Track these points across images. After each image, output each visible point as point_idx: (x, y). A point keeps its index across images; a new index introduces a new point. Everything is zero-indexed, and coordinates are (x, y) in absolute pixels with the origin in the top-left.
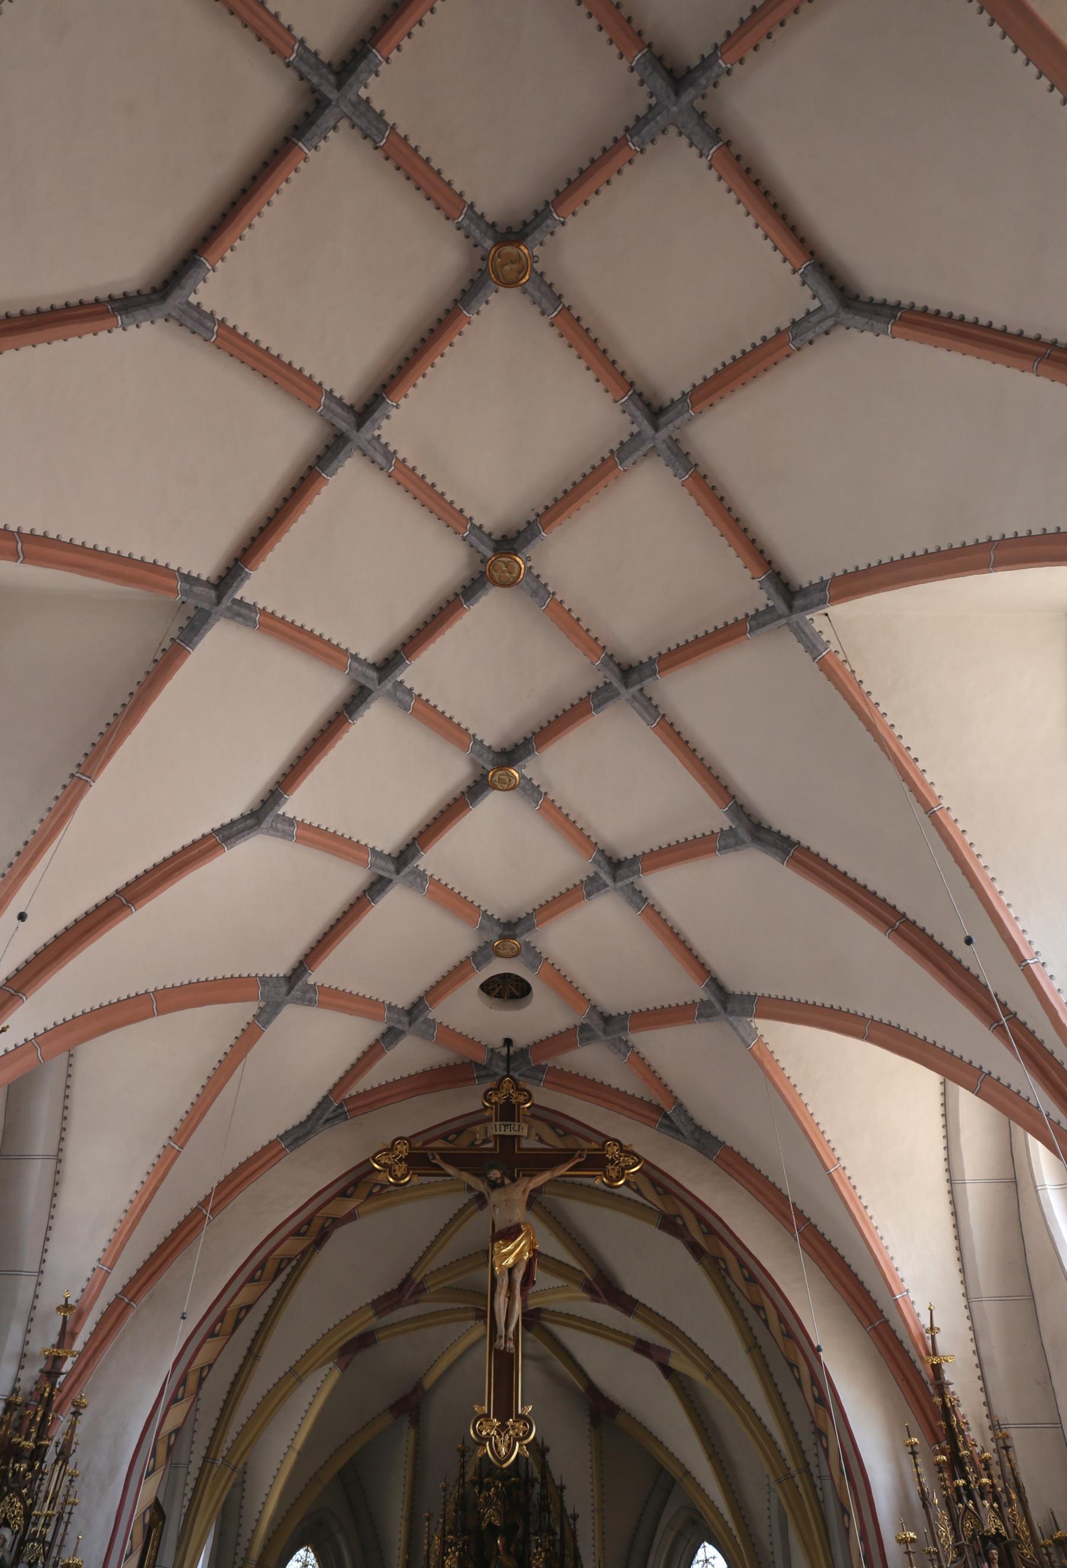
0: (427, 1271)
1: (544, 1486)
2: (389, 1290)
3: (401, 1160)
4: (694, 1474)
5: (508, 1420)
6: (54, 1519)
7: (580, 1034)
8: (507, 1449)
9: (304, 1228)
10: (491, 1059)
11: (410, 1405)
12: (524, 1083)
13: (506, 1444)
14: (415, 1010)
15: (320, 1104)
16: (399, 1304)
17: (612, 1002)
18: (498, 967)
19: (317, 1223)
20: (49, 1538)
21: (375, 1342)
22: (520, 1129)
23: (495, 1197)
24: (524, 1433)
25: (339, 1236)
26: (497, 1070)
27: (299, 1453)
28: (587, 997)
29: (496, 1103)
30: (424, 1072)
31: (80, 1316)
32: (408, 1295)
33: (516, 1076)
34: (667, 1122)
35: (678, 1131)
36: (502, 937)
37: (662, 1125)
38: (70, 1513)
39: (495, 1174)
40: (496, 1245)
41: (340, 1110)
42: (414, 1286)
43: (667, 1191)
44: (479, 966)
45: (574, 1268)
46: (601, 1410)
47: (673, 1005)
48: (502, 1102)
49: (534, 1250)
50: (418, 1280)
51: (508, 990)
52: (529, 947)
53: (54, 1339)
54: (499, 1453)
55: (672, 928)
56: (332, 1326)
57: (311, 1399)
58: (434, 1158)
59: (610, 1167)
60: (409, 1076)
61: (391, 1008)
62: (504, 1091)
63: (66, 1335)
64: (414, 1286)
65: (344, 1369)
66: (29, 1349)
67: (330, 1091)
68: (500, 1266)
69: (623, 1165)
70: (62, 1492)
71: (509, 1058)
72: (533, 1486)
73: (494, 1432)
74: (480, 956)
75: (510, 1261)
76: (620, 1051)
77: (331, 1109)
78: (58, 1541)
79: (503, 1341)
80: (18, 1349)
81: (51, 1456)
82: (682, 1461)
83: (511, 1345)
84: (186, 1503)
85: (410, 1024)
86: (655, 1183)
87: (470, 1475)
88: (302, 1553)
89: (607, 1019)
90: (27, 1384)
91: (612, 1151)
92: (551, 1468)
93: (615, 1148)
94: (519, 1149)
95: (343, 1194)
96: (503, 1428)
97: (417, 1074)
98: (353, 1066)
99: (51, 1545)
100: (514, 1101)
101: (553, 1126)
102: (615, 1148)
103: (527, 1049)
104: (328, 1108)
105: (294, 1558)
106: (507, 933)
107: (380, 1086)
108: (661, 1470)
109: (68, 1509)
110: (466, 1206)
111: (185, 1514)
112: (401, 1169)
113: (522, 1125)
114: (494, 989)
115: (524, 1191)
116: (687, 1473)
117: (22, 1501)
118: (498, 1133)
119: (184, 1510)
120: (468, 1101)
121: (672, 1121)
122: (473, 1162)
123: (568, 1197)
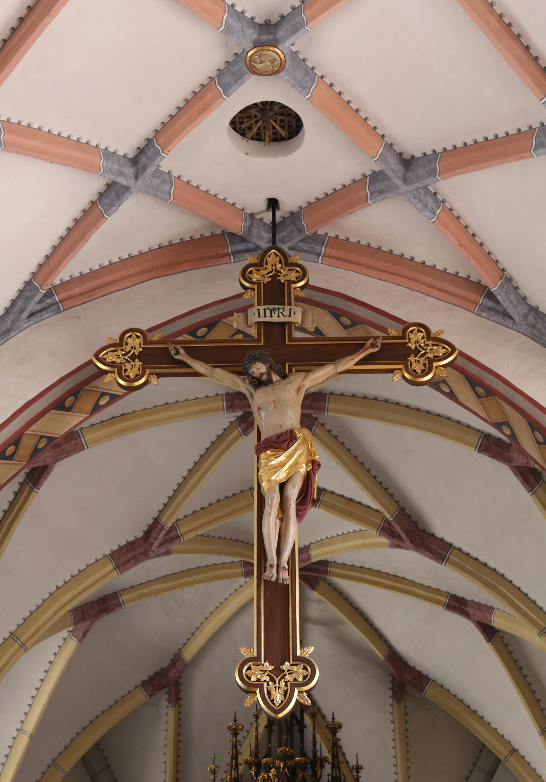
0: (179, 514)
1: (335, 765)
2: (131, 539)
3: (133, 357)
4: (522, 752)
5: (283, 664)
7: (373, 185)
8: (282, 699)
9: (11, 449)
10: (250, 227)
11: (168, 680)
12: (295, 257)
13: (282, 691)
14: (141, 158)
15: (21, 292)
16: (146, 555)
17: (415, 140)
18: (254, 91)
19: (27, 445)
21: (119, 605)
22: (295, 315)
23: (259, 398)
24: (305, 677)
25: (64, 473)
26: (259, 243)
27: (31, 736)
28: (380, 132)
29: (258, 283)
30: (161, 247)
32: (157, 543)
33: (285, 248)
34: (491, 304)
35: (506, 315)
36: (258, 44)
37: (483, 308)
39: (259, 369)
40: (262, 456)
41: (49, 301)
42: (163, 533)
43: (490, 392)
44: (227, 89)
45: (369, 507)
46: (405, 681)
47: (501, 134)
48: (267, 280)
49: (313, 462)
50: (169, 525)
51: (270, 126)
52: (299, 61)
54: (272, 701)
55: (501, 16)
56: (61, 584)
57: (42, 675)
58: (178, 353)
59: (412, 359)
60: (141, 254)
61: (108, 154)
62: (269, 267)
64: (163, 533)
67: (34, 274)
68: (269, 480)
69: (430, 355)
71: (274, 227)
72: (322, 766)
73: (266, 678)
74: (227, 76)
75: (281, 475)
76: (426, 206)
77: (37, 298)
79: (274, 570)
82: (507, 737)
83: (285, 575)
85: (136, 177)
86: (473, 382)
87: (245, 755)
89: (408, 163)
91: (416, 339)
92: (345, 749)
93: (421, 335)
94: (291, 339)
95: (59, 405)
96: (278, 672)
97: (151, 250)
98: (62, 239)
100: (282, 279)
101: (336, 314)
102: (421, 335)
103: (299, 213)
104: (33, 297)
106: (264, 38)
107: (102, 268)
108: (482, 748)
110: (226, 431)
112: (133, 368)
113: (294, 308)
114: (250, 128)
115: (298, 390)
116: (514, 751)
118: (262, 319)
120: (221, 283)
121: (498, 302)
122: (231, 357)
123: (357, 414)
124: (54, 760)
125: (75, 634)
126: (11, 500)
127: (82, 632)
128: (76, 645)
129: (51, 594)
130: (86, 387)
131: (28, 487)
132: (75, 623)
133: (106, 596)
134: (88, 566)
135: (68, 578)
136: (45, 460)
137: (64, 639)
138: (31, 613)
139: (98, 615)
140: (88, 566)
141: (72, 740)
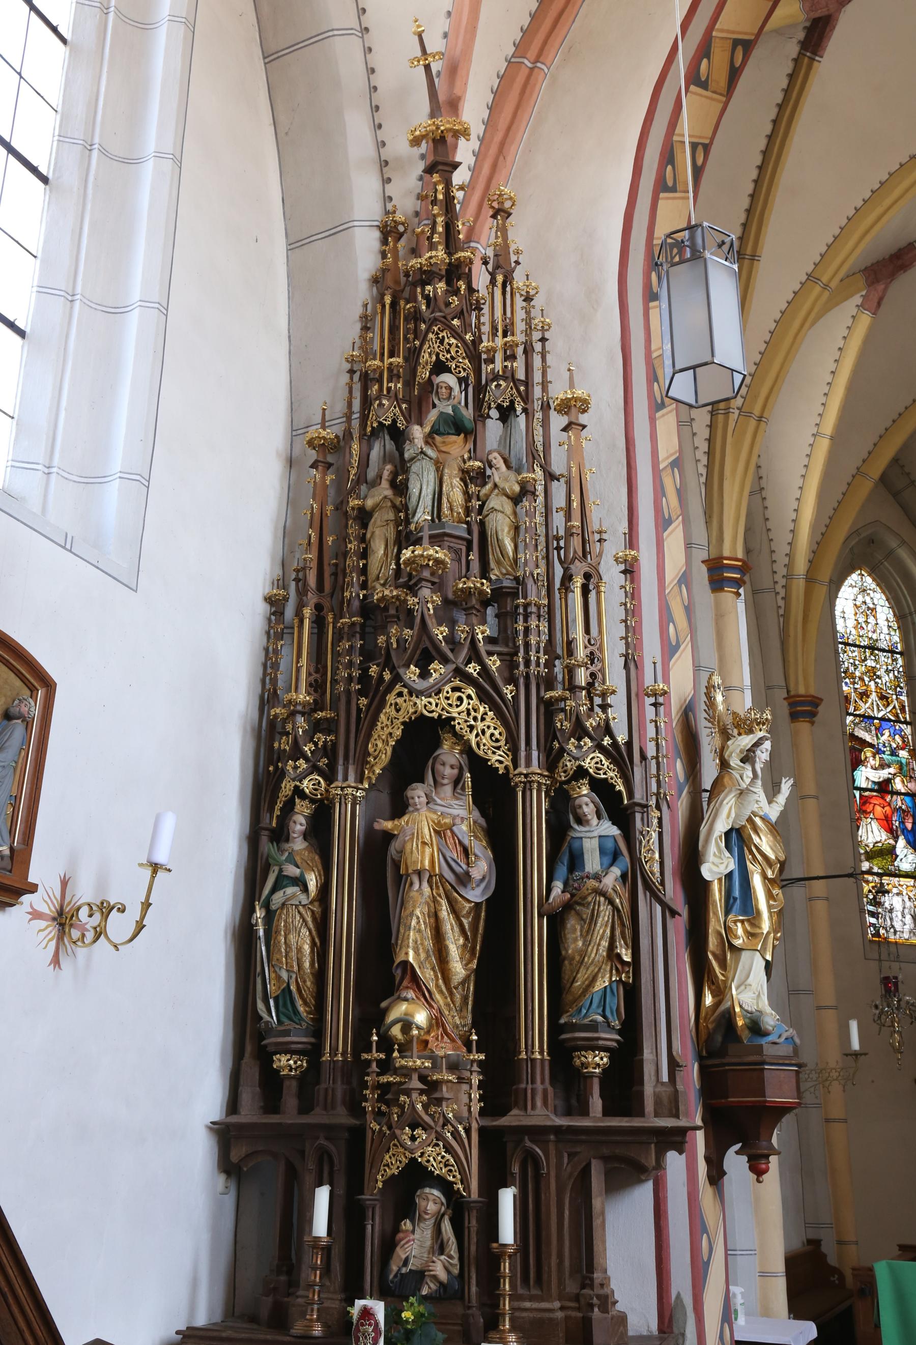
6: (520, 350)
20: (521, 375)
27: (832, 438)
31: (455, 69)
38: (543, 340)
53: (426, 107)
57: (833, 367)
63: (444, 102)
65: (875, 305)
66: (386, 153)
70: (520, 315)
78: (537, 377)
80: (370, 150)
81: (481, 279)
84: (703, 471)
88: (854, 577)
90: (405, 203)
99: (527, 383)
105: (846, 583)
109: (536, 335)
111: (706, 484)
117: (455, 334)
119: (703, 479)
124: (858, 469)
125: (866, 307)
126: (785, 87)
127: (876, 300)
128: (869, 319)
129: (849, 219)
130: (667, 592)
131: (806, 59)
132: (869, 286)
133: (900, 250)
134: (891, 175)
135: (868, 194)
136: (827, 6)
137: (853, 317)
138: (829, 246)
139: (892, 276)
140: (891, 175)
141: (875, 445)
